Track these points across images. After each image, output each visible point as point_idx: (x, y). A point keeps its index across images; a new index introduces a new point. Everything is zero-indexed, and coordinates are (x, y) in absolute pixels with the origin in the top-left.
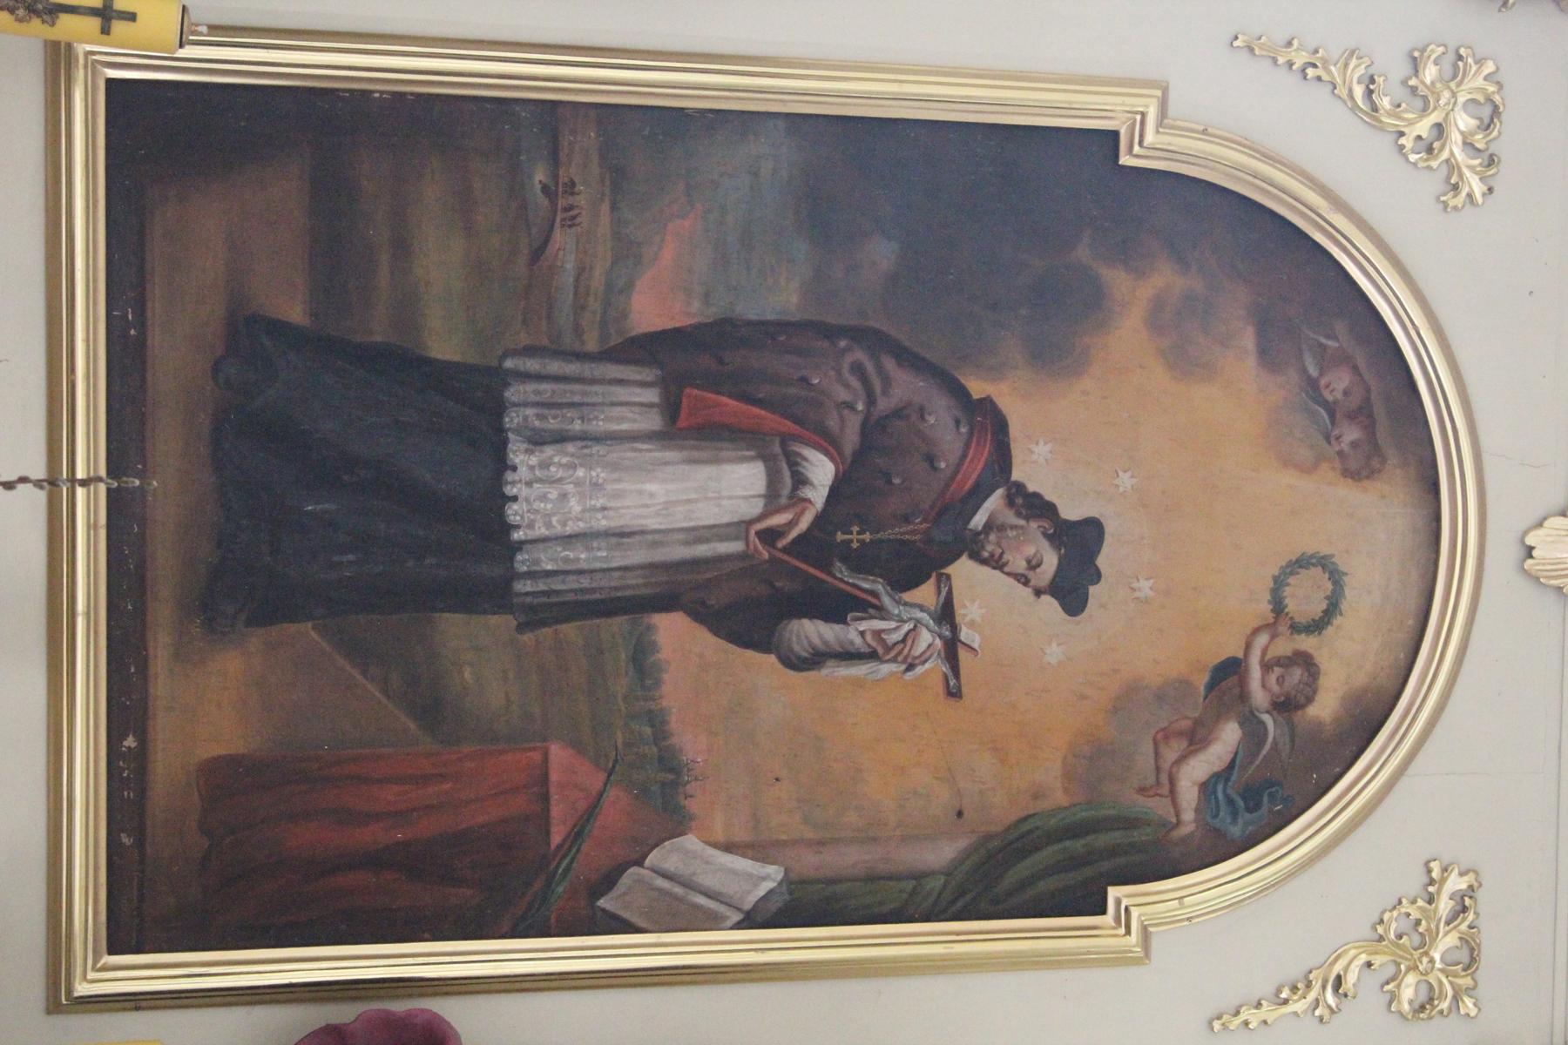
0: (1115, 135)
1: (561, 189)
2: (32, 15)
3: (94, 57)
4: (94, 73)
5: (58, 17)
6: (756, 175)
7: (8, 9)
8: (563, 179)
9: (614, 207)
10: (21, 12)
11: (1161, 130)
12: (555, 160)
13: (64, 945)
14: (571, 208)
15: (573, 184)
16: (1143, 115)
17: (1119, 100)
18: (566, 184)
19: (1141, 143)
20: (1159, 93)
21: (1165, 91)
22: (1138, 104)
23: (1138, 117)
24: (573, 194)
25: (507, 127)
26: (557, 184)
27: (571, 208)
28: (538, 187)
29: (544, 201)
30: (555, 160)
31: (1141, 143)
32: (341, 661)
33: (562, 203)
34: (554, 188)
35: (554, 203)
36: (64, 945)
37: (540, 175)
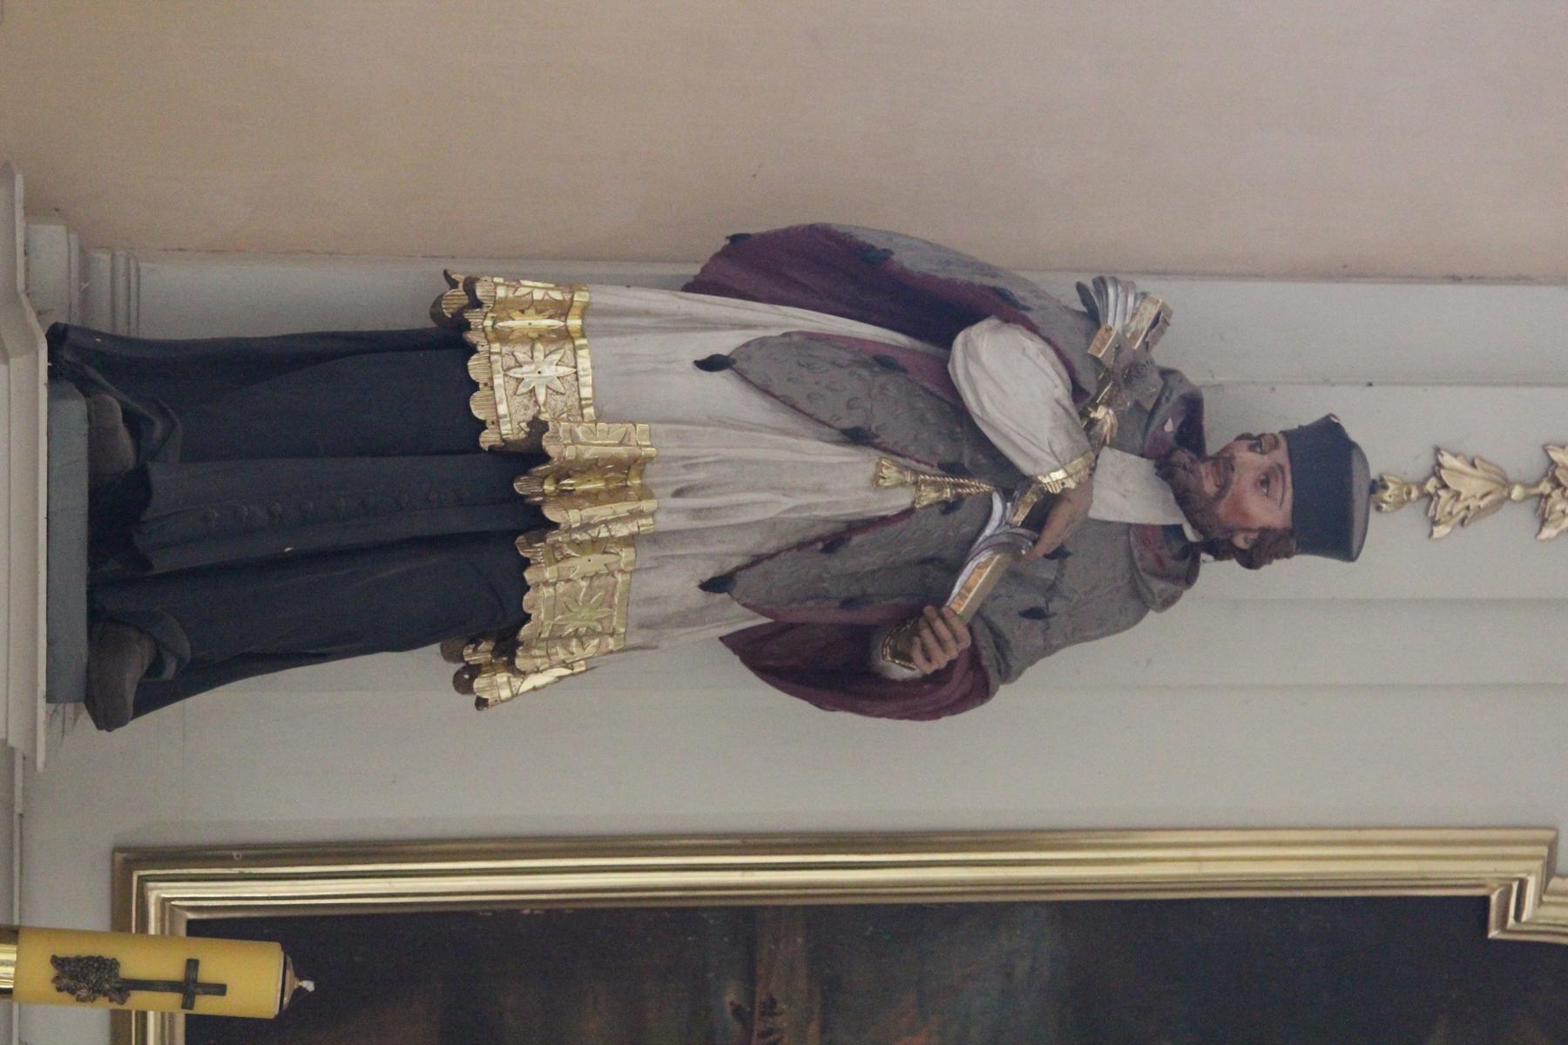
0: (1485, 901)
1: (757, 1011)
2: (97, 995)
3: (173, 903)
4: (171, 917)
5: (129, 995)
6: (1009, 976)
7: (68, 990)
8: (761, 997)
9: (825, 1028)
10: (83, 993)
11: (1545, 898)
12: (750, 978)
13: (185, 871)
14: (770, 1032)
15: (773, 1002)
16: (1523, 884)
17: (1490, 866)
18: (764, 1003)
19: (1518, 917)
20: (1544, 851)
21: (1552, 845)
22: (1515, 868)
23: (1515, 886)
24: (772, 1015)
25: (690, 938)
26: (752, 1003)
27: (770, 1032)
28: (729, 1009)
29: (735, 1027)
30: (750, 978)
31: (1518, 917)
32: (1098, 305)
33: (759, 1027)
34: (748, 1009)
35: (748, 1030)
36: (185, 871)
37: (731, 996)
